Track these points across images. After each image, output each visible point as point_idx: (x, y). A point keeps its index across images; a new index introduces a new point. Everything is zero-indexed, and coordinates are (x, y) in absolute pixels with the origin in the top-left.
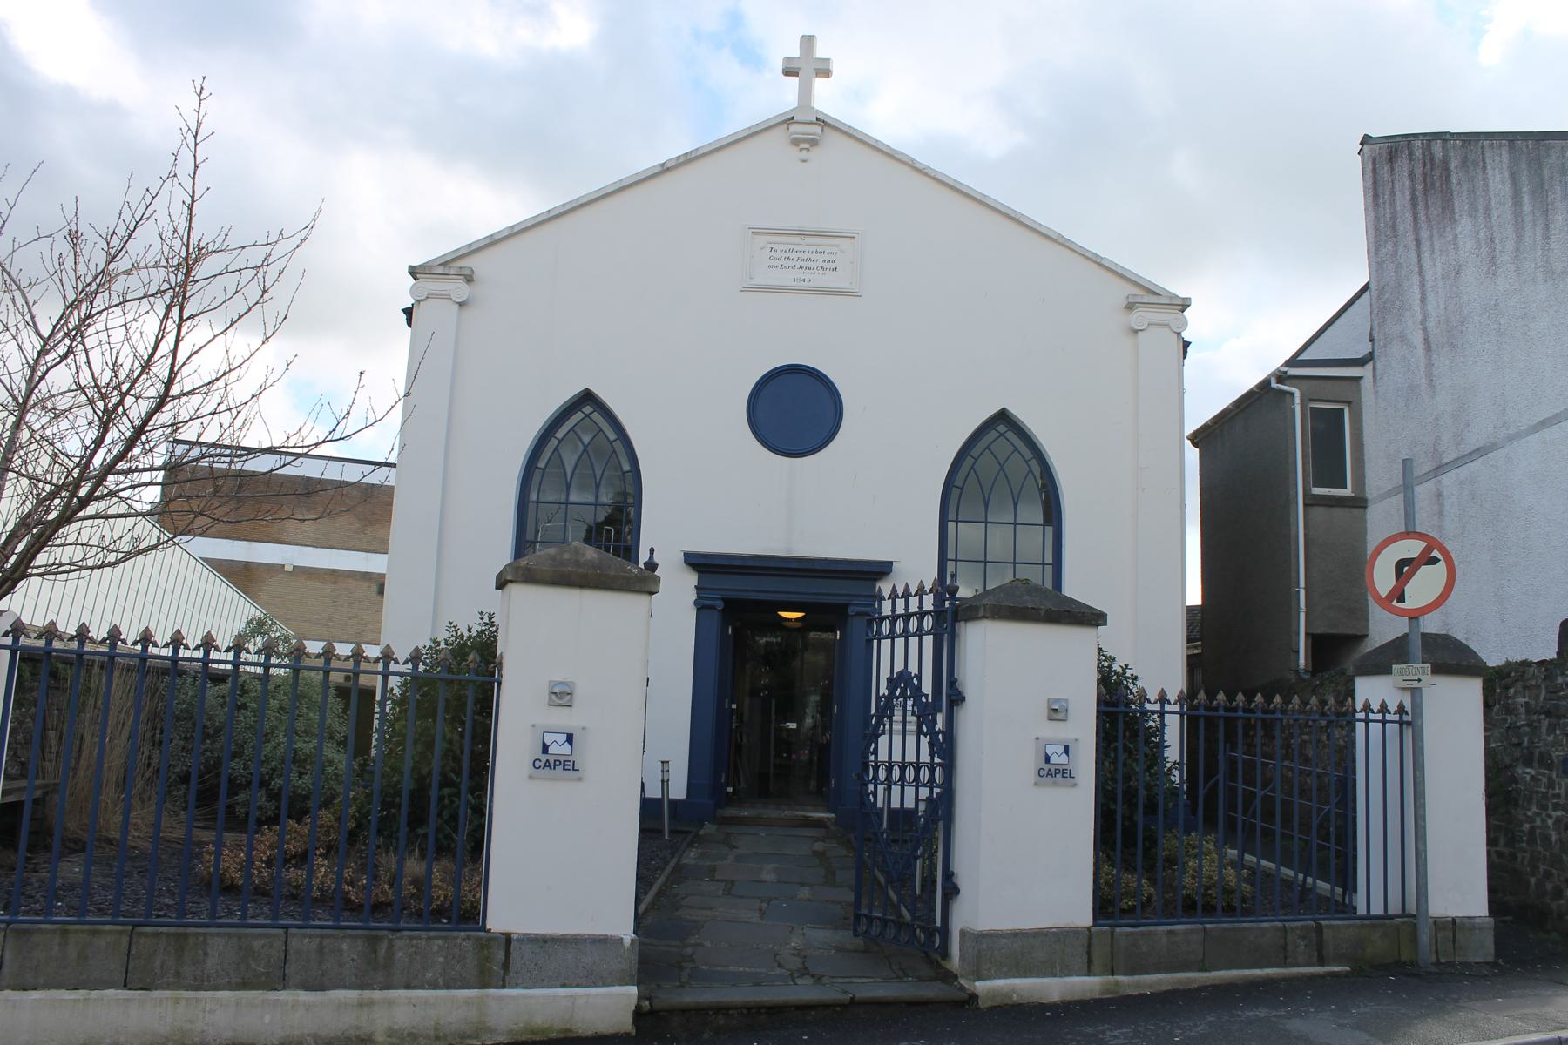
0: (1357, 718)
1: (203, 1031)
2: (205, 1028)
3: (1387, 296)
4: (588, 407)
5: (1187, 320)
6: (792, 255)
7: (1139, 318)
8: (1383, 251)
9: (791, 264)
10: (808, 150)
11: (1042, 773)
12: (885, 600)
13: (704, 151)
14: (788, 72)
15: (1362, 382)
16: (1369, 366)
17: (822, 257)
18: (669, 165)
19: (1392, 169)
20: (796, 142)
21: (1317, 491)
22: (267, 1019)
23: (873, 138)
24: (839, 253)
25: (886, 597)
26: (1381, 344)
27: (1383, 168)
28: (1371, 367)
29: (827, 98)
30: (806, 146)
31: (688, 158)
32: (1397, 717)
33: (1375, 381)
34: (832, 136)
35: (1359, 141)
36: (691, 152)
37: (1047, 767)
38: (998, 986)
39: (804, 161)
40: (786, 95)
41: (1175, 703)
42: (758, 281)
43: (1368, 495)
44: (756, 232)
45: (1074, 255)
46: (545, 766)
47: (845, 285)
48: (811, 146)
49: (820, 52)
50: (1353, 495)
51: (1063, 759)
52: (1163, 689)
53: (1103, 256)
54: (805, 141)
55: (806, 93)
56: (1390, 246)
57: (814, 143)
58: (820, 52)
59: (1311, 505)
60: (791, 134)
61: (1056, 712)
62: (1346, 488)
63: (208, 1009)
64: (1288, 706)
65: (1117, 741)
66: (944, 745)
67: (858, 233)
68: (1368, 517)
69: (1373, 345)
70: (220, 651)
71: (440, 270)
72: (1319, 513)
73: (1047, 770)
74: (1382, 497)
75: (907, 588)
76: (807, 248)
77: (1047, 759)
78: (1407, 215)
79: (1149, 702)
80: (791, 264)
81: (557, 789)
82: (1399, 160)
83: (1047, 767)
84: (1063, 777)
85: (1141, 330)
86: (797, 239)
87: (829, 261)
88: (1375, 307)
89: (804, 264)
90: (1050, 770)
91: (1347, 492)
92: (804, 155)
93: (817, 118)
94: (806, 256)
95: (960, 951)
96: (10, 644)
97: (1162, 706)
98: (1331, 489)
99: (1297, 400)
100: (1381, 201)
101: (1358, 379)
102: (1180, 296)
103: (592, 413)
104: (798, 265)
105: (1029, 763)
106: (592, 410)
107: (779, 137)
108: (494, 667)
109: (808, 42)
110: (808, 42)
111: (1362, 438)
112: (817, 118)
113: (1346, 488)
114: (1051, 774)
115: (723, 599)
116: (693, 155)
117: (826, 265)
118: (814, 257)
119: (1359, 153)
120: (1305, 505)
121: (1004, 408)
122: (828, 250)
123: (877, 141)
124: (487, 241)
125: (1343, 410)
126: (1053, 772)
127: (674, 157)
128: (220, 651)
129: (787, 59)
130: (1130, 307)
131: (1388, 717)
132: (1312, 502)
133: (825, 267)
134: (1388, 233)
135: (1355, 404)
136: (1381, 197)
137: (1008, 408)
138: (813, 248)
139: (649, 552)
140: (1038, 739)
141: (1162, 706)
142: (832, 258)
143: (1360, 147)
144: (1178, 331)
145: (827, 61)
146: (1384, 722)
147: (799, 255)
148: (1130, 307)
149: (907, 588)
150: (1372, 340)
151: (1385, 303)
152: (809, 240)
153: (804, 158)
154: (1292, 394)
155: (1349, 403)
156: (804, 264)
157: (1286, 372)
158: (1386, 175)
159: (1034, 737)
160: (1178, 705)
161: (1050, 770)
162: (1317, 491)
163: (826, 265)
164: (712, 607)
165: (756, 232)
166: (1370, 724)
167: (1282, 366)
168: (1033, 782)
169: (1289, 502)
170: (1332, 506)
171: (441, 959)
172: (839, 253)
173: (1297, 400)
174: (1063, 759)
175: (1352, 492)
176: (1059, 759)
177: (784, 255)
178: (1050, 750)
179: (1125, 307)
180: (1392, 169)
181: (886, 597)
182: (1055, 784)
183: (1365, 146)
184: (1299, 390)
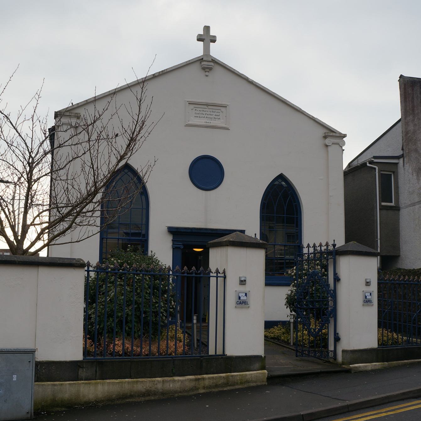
0: (211, 275)
1: (154, 390)
2: (155, 389)
3: (409, 135)
4: (126, 170)
5: (345, 143)
6: (204, 113)
7: (328, 141)
8: (408, 118)
9: (203, 116)
10: (208, 72)
11: (238, 303)
12: (304, 248)
13: (306, 114)
14: (199, 40)
15: (398, 164)
16: (401, 160)
17: (214, 114)
18: (156, 75)
19: (413, 89)
20: (204, 69)
21: (383, 204)
22: (171, 386)
23: (233, 68)
24: (221, 112)
25: (305, 247)
26: (407, 152)
27: (409, 89)
28: (402, 160)
29: (216, 51)
30: (208, 70)
31: (164, 72)
32: (215, 275)
33: (404, 165)
34: (217, 68)
35: (399, 77)
36: (165, 70)
37: (239, 301)
38: (356, 366)
39: (207, 76)
40: (198, 50)
41: (215, 273)
42: (190, 123)
43: (400, 206)
44: (190, 103)
45: (305, 117)
46: (240, 303)
47: (223, 125)
48: (210, 70)
49: (212, 33)
50: (395, 205)
51: (245, 298)
52: (217, 268)
53: (316, 117)
54: (208, 68)
55: (207, 49)
56: (411, 117)
57: (211, 69)
58: (212, 33)
59: (382, 209)
60: (203, 65)
61: (368, 284)
62: (392, 203)
63: (155, 383)
64: (206, 272)
65: (238, 293)
66: (333, 294)
67: (228, 105)
68: (400, 213)
69: (403, 152)
70: (220, 273)
71: (68, 114)
72: (384, 212)
73: (239, 302)
74: (407, 207)
75: (308, 245)
76: (209, 110)
77: (240, 298)
78: (419, 107)
79: (212, 273)
80: (203, 116)
81: (242, 312)
82: (416, 86)
83: (239, 301)
84: (245, 304)
85: (330, 145)
86: (205, 107)
87: (217, 115)
88: (404, 138)
89: (208, 116)
90: (240, 302)
91: (393, 204)
92: (207, 73)
93: (212, 60)
94: (209, 113)
95: (342, 356)
96: (87, 269)
97: (217, 274)
98: (388, 203)
99: (377, 171)
100: (408, 100)
101: (397, 164)
102: (343, 133)
103: (128, 172)
104: (206, 116)
105: (361, 299)
106: (128, 171)
107: (197, 65)
108: (401, 281)
109: (207, 29)
110: (207, 29)
111: (398, 185)
112: (212, 60)
113: (392, 203)
114: (241, 303)
115: (182, 245)
116: (165, 72)
117: (216, 117)
118: (212, 113)
119: (398, 81)
120: (380, 209)
121: (282, 173)
122: (217, 111)
123: (234, 69)
124: (85, 102)
125: (391, 175)
126: (367, 302)
127: (158, 72)
128: (220, 273)
129: (199, 35)
130: (325, 137)
131: (219, 275)
132: (382, 208)
133: (216, 118)
134: (411, 112)
135: (395, 173)
136: (408, 98)
137: (283, 173)
138: (211, 110)
139: (254, 235)
140: (363, 291)
141: (217, 274)
142: (218, 114)
143: (399, 79)
144: (342, 146)
145: (215, 37)
146: (217, 277)
147: (206, 112)
148: (325, 137)
149: (308, 245)
150: (403, 149)
151: (409, 137)
152: (210, 107)
153: (207, 75)
154: (375, 169)
155: (394, 172)
156: (208, 116)
157: (373, 161)
158: (410, 91)
159: (235, 290)
160: (216, 274)
161: (240, 302)
162: (383, 204)
163: (216, 117)
164: (179, 248)
165: (190, 103)
166: (218, 278)
167: (372, 158)
168: (235, 306)
169: (374, 208)
170: (388, 210)
171: (215, 365)
172: (221, 112)
173: (377, 171)
174: (245, 298)
175: (395, 204)
176: (243, 298)
177: (200, 112)
178: (240, 295)
179: (323, 137)
180: (413, 89)
181: (305, 247)
182: (242, 308)
183: (401, 79)
184: (378, 167)
